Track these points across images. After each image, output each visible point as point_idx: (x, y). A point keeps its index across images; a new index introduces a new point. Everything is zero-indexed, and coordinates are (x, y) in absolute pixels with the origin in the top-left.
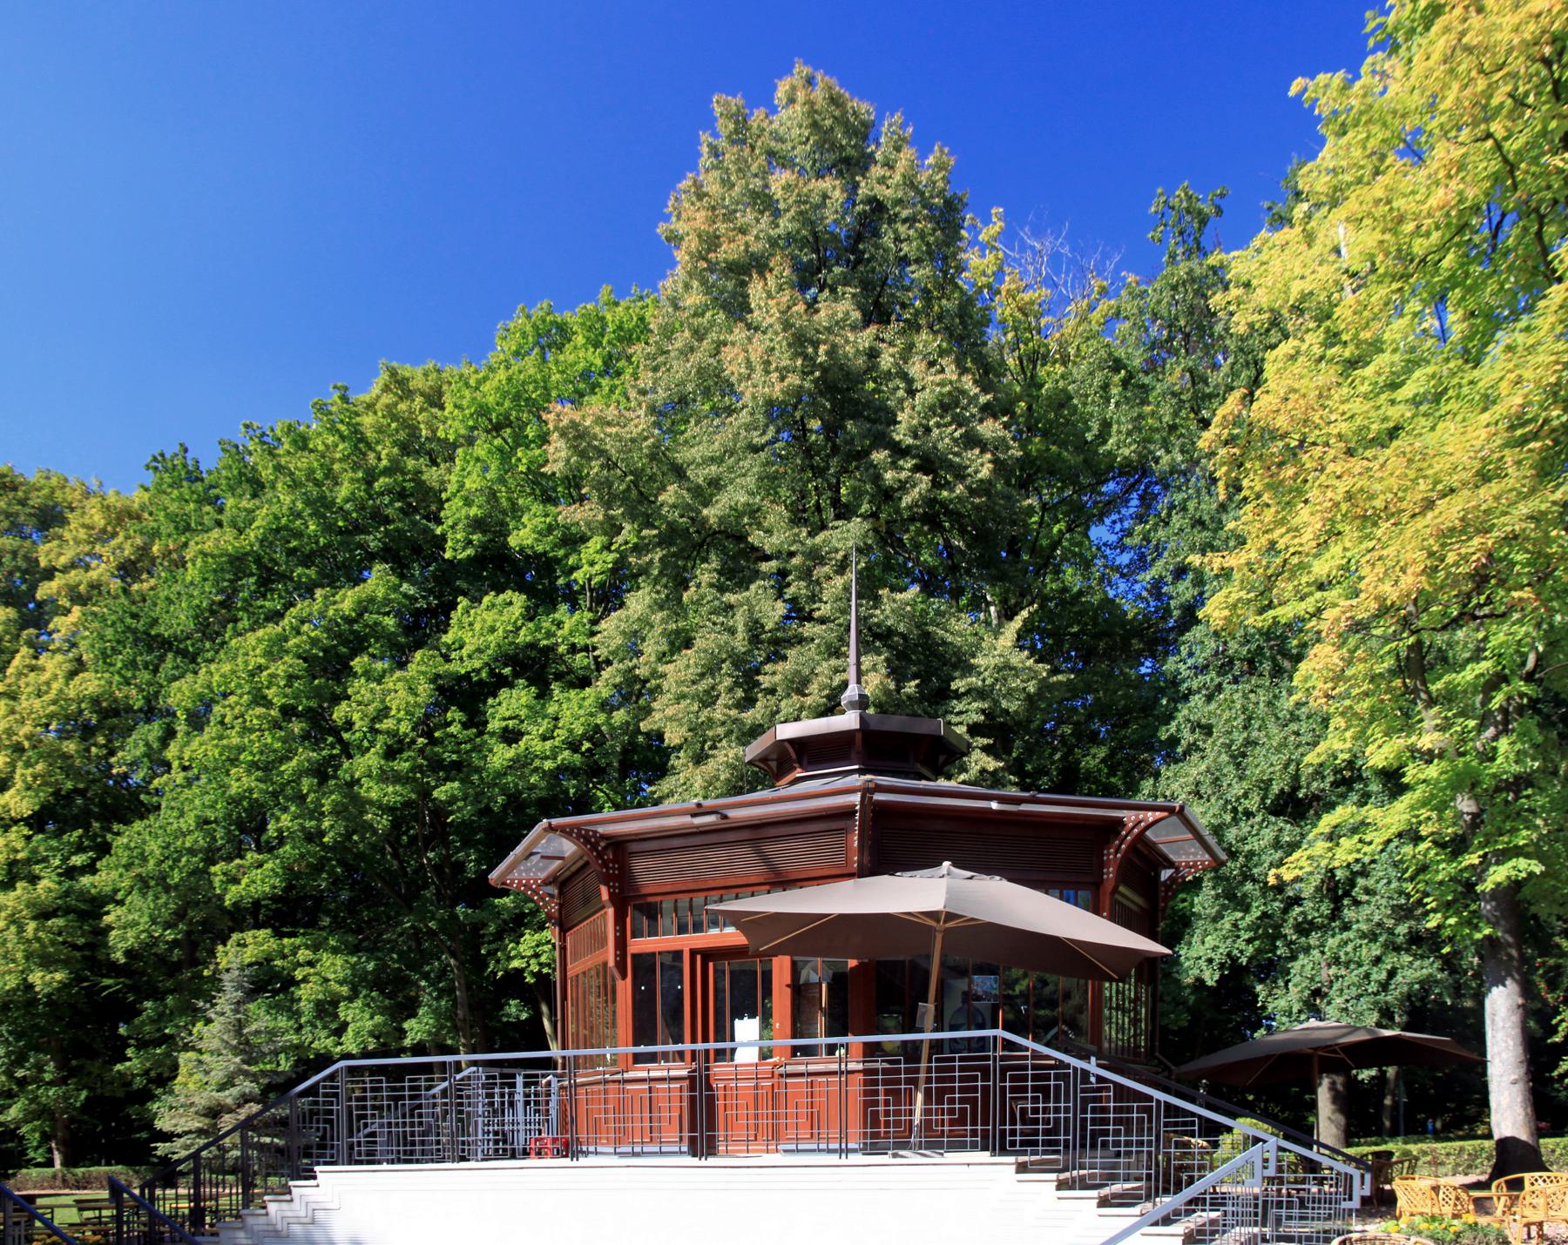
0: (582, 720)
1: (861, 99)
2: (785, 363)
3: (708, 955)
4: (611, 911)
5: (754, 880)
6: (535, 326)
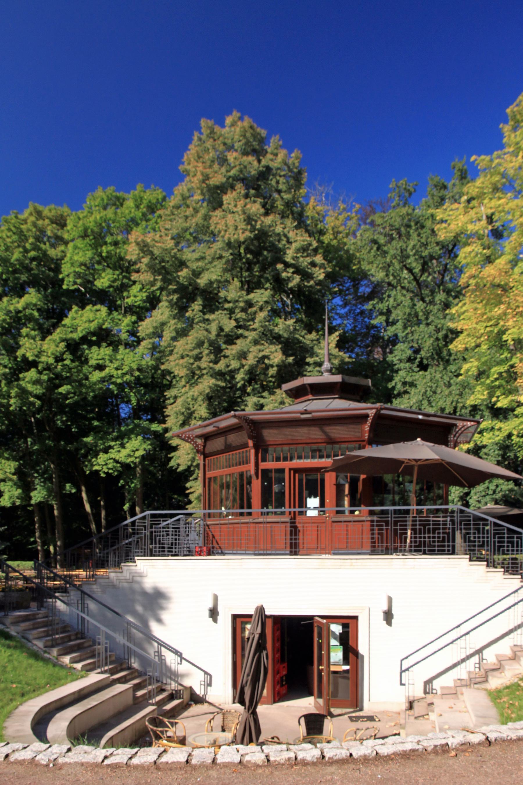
0: (136, 362)
1: (262, 128)
2: (244, 227)
3: (296, 471)
4: (253, 451)
5: (319, 441)
6: (108, 196)
